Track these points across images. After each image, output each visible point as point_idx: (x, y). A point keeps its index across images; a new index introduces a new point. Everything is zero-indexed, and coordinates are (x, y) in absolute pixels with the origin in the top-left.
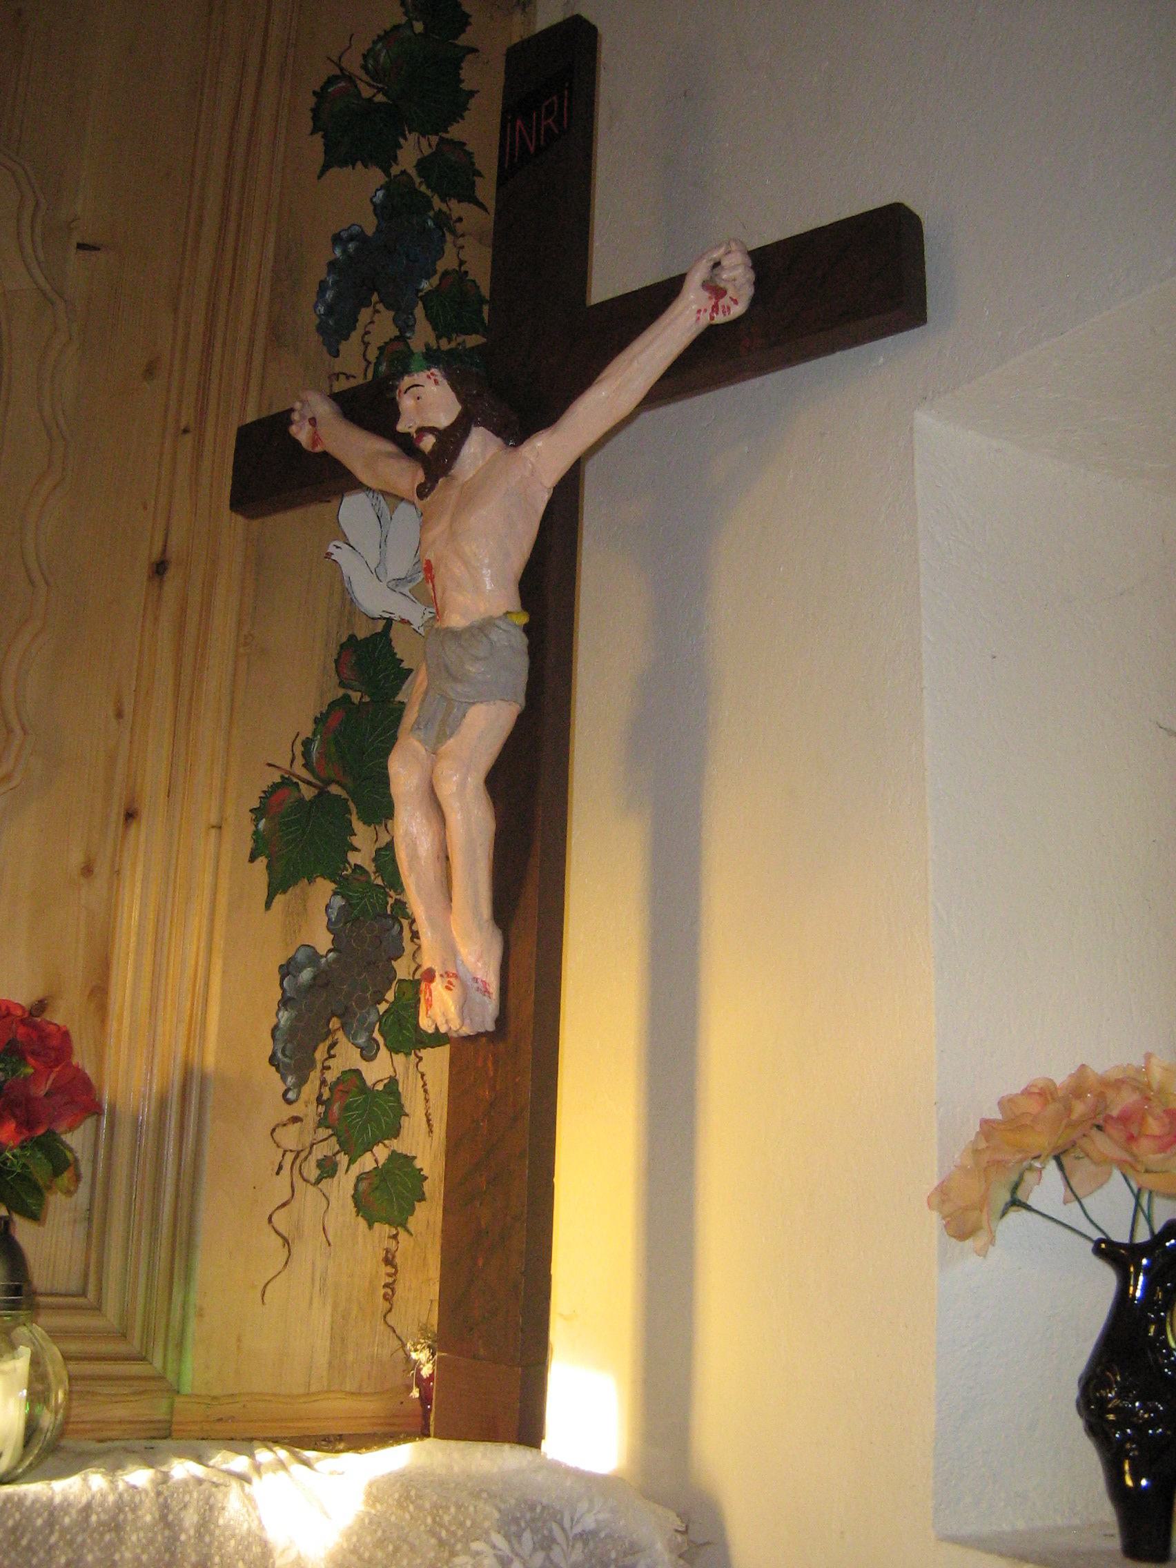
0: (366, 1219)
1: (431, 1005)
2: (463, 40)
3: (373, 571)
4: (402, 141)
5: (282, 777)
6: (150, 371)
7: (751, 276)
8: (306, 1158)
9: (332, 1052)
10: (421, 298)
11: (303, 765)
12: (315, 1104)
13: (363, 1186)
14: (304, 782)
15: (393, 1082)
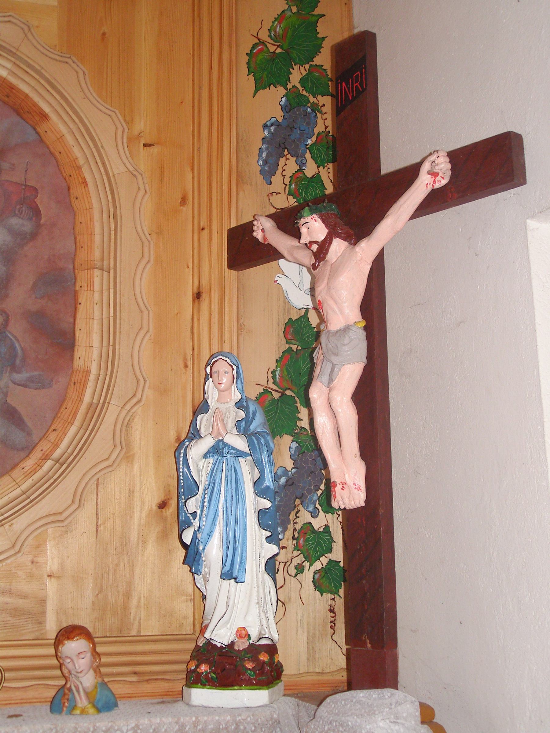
0: (319, 592)
1: (336, 497)
2: (317, 12)
3: (297, 287)
4: (291, 70)
5: (264, 389)
6: (184, 201)
7: (449, 166)
8: (289, 565)
9: (298, 515)
10: (308, 148)
11: (273, 383)
12: (292, 540)
13: (317, 576)
14: (274, 391)
15: (327, 527)
